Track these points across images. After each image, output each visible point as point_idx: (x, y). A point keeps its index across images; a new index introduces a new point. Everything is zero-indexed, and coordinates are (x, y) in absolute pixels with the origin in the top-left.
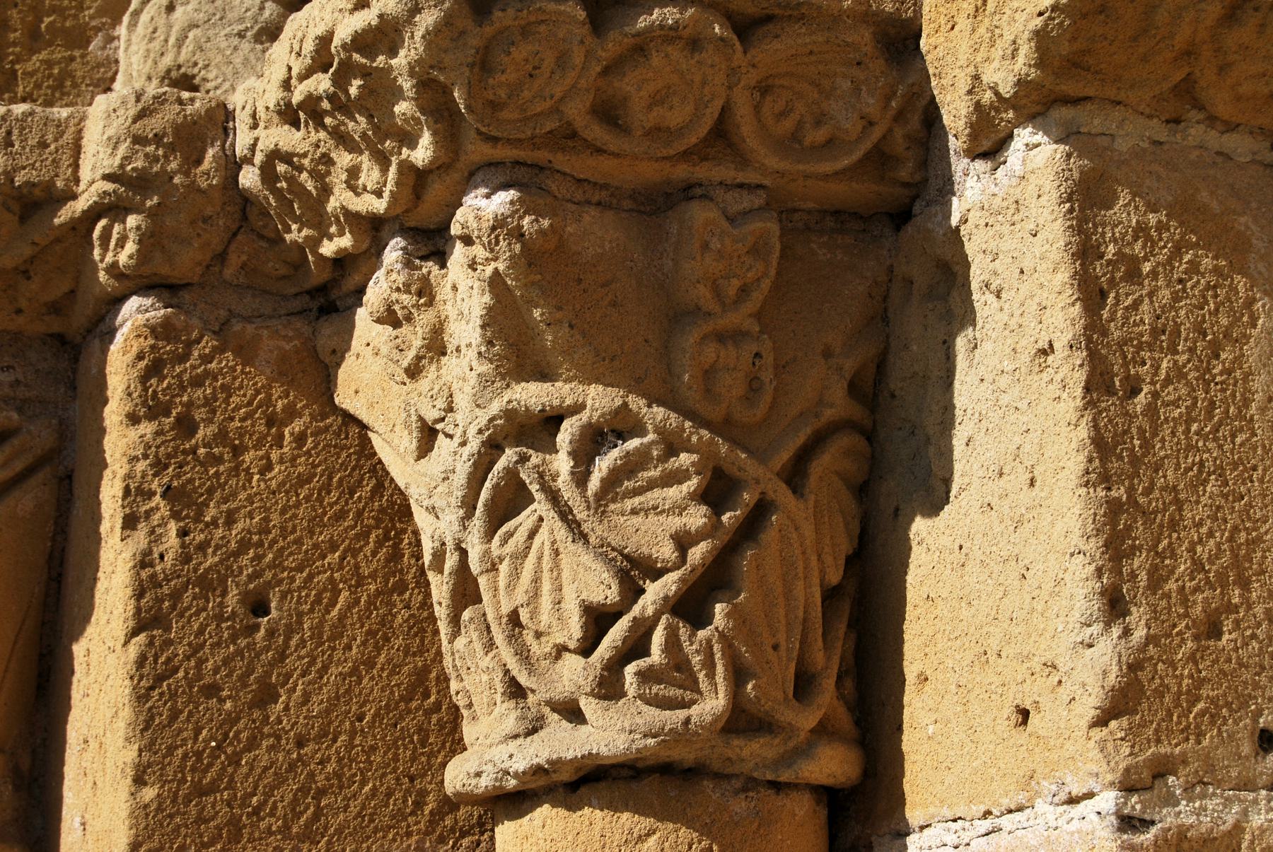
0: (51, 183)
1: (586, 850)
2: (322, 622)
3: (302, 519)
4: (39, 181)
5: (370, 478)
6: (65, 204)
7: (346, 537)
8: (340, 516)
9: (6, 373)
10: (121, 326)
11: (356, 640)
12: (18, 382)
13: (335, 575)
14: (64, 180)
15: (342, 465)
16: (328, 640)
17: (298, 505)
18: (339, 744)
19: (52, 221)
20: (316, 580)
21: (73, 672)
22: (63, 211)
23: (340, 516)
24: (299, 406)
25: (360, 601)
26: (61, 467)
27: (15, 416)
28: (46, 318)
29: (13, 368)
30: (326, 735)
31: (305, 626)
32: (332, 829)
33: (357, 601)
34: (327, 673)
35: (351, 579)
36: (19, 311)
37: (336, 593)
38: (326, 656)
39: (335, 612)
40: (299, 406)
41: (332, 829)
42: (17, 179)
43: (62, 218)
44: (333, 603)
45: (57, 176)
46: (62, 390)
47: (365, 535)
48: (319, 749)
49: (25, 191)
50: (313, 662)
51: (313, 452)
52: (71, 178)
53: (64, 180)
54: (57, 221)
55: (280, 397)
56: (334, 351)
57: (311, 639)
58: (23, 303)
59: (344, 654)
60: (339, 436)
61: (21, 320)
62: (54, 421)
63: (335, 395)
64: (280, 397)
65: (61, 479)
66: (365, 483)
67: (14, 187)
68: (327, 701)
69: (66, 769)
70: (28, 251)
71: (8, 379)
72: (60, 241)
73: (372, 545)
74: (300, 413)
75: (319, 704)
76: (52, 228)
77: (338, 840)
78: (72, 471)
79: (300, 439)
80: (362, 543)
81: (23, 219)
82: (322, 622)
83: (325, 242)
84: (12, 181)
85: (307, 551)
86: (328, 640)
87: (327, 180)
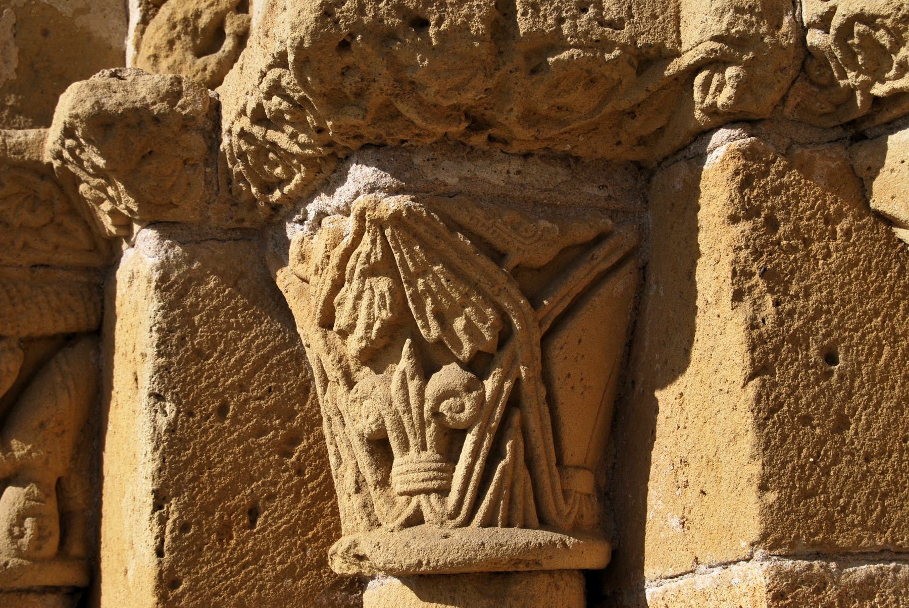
2: (874, 369)
3: (854, 293)
5: (896, 262)
7: (884, 306)
8: (879, 290)
11: (897, 382)
13: (880, 334)
15: (877, 252)
16: (879, 383)
17: (850, 283)
18: (893, 459)
20: (867, 338)
23: (879, 290)
24: (844, 209)
25: (897, 354)
30: (883, 453)
31: (863, 372)
32: (894, 523)
33: (896, 354)
34: (880, 407)
35: (890, 337)
37: (881, 347)
38: (879, 394)
39: (882, 362)
40: (844, 209)
41: (894, 523)
44: (880, 355)
47: (896, 305)
48: (880, 463)
50: (870, 400)
51: (857, 243)
55: (832, 203)
56: (869, 168)
57: (868, 382)
59: (890, 392)
60: (873, 231)
63: (871, 201)
64: (832, 203)
66: (893, 266)
68: (883, 428)
73: (901, 312)
74: (845, 215)
75: (878, 430)
77: (898, 531)
79: (847, 233)
80: (895, 310)
82: (874, 369)
83: (877, 85)
85: (859, 317)
86: (879, 383)
87: (903, 35)
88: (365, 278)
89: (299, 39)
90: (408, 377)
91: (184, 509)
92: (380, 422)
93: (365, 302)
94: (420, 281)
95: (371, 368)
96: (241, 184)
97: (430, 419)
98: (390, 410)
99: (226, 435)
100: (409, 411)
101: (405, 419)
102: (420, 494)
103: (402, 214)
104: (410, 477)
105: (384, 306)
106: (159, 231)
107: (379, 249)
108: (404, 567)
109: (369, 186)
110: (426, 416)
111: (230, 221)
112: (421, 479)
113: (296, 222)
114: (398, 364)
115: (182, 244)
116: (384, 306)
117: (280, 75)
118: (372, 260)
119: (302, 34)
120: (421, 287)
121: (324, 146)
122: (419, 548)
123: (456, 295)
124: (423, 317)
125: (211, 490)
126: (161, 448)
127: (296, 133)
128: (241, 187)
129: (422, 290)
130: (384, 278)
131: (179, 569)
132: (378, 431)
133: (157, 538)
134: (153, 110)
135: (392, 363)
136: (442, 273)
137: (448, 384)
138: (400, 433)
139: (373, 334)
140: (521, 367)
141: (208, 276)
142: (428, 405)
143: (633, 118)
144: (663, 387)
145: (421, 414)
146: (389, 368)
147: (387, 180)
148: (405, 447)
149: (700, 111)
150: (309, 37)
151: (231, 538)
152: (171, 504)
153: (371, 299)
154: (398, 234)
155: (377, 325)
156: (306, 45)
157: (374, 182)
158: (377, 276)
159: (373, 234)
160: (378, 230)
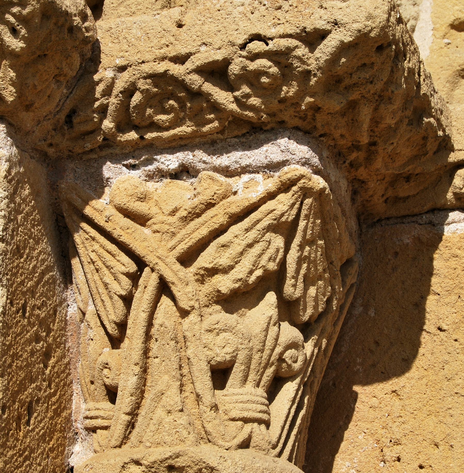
10: (449, 224)
88: (267, 232)
89: (370, 28)
90: (272, 322)
92: (235, 354)
93: (257, 249)
94: (307, 248)
95: (223, 307)
96: (95, 115)
97: (275, 362)
98: (248, 346)
99: (25, 333)
100: (262, 351)
101: (256, 357)
102: (254, 423)
103: (325, 191)
104: (250, 406)
105: (274, 260)
106: (7, 128)
107: (294, 211)
109: (304, 160)
110: (272, 359)
112: (258, 410)
113: (124, 165)
114: (250, 310)
115: (17, 147)
116: (274, 260)
117: (297, 46)
118: (283, 219)
119: (374, 25)
120: (306, 254)
123: (320, 268)
124: (296, 277)
125: (17, 380)
127: (251, 94)
128: (94, 117)
129: (305, 256)
130: (280, 237)
132: (230, 361)
134: (74, 20)
135: (245, 308)
136: (322, 248)
137: (296, 337)
138: (247, 367)
139: (253, 278)
140: (324, 340)
141: (26, 183)
142: (278, 350)
143: (406, 182)
144: (367, 382)
145: (270, 356)
146: (241, 312)
147: (316, 160)
148: (245, 380)
149: (452, 194)
150: (379, 30)
151: (20, 431)
153: (264, 250)
154: (315, 205)
155: (259, 273)
156: (372, 35)
158: (275, 233)
159: (296, 199)
160: (302, 197)
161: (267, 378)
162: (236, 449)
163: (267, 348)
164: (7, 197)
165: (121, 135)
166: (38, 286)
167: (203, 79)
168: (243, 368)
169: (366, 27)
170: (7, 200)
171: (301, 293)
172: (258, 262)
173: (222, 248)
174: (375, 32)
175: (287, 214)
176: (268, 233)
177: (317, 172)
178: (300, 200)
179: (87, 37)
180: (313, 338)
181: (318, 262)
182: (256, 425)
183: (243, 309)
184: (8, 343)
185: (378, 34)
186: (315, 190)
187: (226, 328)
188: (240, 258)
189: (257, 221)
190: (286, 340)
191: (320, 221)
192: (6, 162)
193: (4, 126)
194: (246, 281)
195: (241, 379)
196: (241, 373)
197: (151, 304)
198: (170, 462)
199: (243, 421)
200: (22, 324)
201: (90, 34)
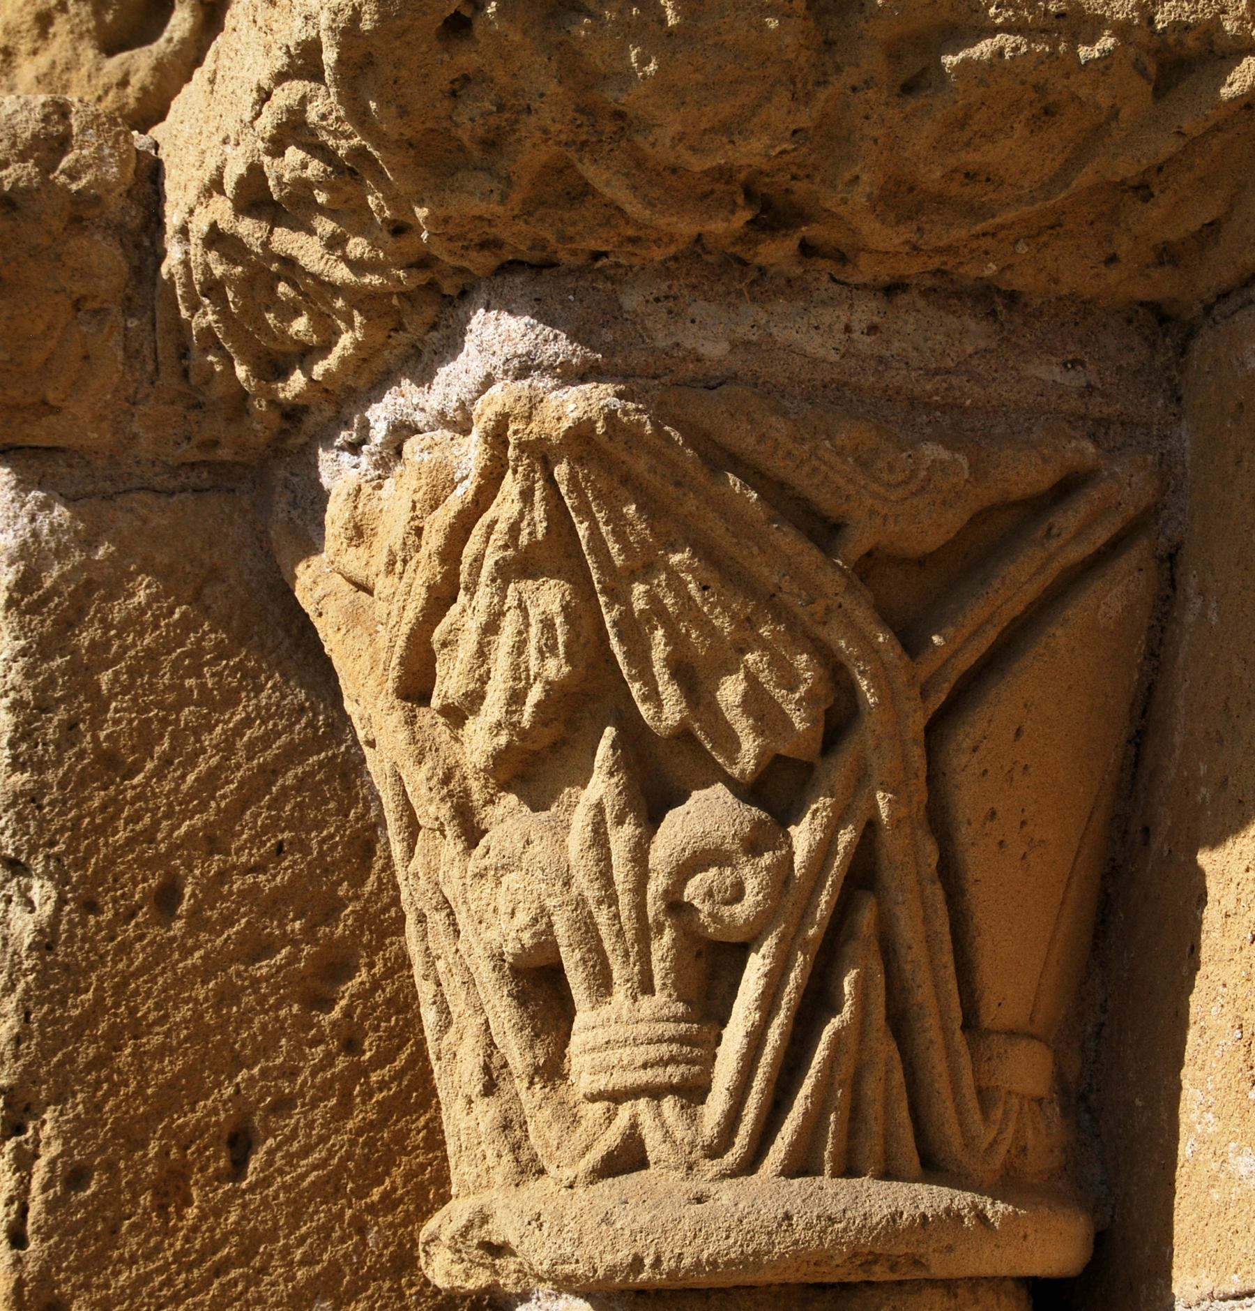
0: (1216, 24)
1: (372, 1308)
4: (1196, 21)
6: (1239, 63)
9: (1072, 373)
12: (1090, 387)
14: (1237, 19)
19: (1217, 91)
21: (1202, 900)
22: (1236, 75)
26: (1162, 539)
27: (1090, 448)
28: (1156, 274)
29: (1083, 364)
36: (1112, 260)
42: (1158, 17)
43: (1235, 87)
45: (1224, 11)
46: (1160, 402)
49: (1171, 39)
52: (1248, 16)
53: (1237, 19)
54: (1226, 92)
58: (1123, 245)
61: (1113, 275)
62: (1150, 457)
65: (1162, 560)
67: (1154, 32)
69: (1188, 1074)
70: (1168, 146)
71: (1076, 383)
72: (1219, 130)
76: (1218, 104)
78: (1178, 547)
81: (1161, 90)
84: (1151, 21)
88: (507, 583)
90: (609, 817)
91: (74, 1133)
92: (541, 926)
95: (520, 797)
97: (662, 918)
98: (567, 898)
99: (176, 956)
101: (602, 917)
102: (637, 1098)
103: (594, 430)
104: (613, 1056)
105: (553, 649)
107: (539, 512)
108: (601, 1272)
109: (516, 362)
110: (651, 912)
111: (185, 446)
112: (639, 1062)
114: (584, 787)
115: (70, 500)
117: (304, 97)
118: (524, 539)
120: (639, 604)
121: (408, 267)
122: (636, 1226)
124: (647, 676)
125: (140, 1089)
126: (20, 987)
128: (212, 363)
129: (642, 611)
130: (552, 582)
131: (62, 1276)
133: (9, 1202)
136: (690, 569)
138: (589, 951)
141: (131, 577)
142: (657, 885)
144: (1216, 841)
146: (564, 797)
147: (560, 347)
148: (602, 984)
152: (44, 1122)
153: (520, 633)
155: (535, 694)
157: (529, 353)
158: (534, 577)
159: (526, 477)
160: (538, 467)
161: (662, 965)
162: (591, 1183)
163: (619, 888)
164: (24, 652)
165: (280, 385)
166: (243, 812)
167: (264, 224)
168: (579, 957)
169: (335, 14)
170: (22, 662)
171: (680, 711)
172: (523, 666)
173: (445, 651)
174: (367, 17)
175: (525, 522)
176: (512, 586)
177: (571, 375)
178: (537, 475)
179: (78, 192)
180: (814, 806)
181: (705, 609)
182: (642, 1103)
183: (567, 790)
184: (75, 1013)
185: (376, 17)
186: (555, 441)
187: (505, 861)
188: (486, 666)
189: (475, 560)
190: (668, 852)
191: (633, 507)
192: (9, 565)
193: (7, 470)
194: (514, 725)
195: (586, 985)
196: (581, 969)
197: (405, 819)
198: (477, 1235)
199: (608, 1099)
200: (151, 943)
201: (84, 181)
